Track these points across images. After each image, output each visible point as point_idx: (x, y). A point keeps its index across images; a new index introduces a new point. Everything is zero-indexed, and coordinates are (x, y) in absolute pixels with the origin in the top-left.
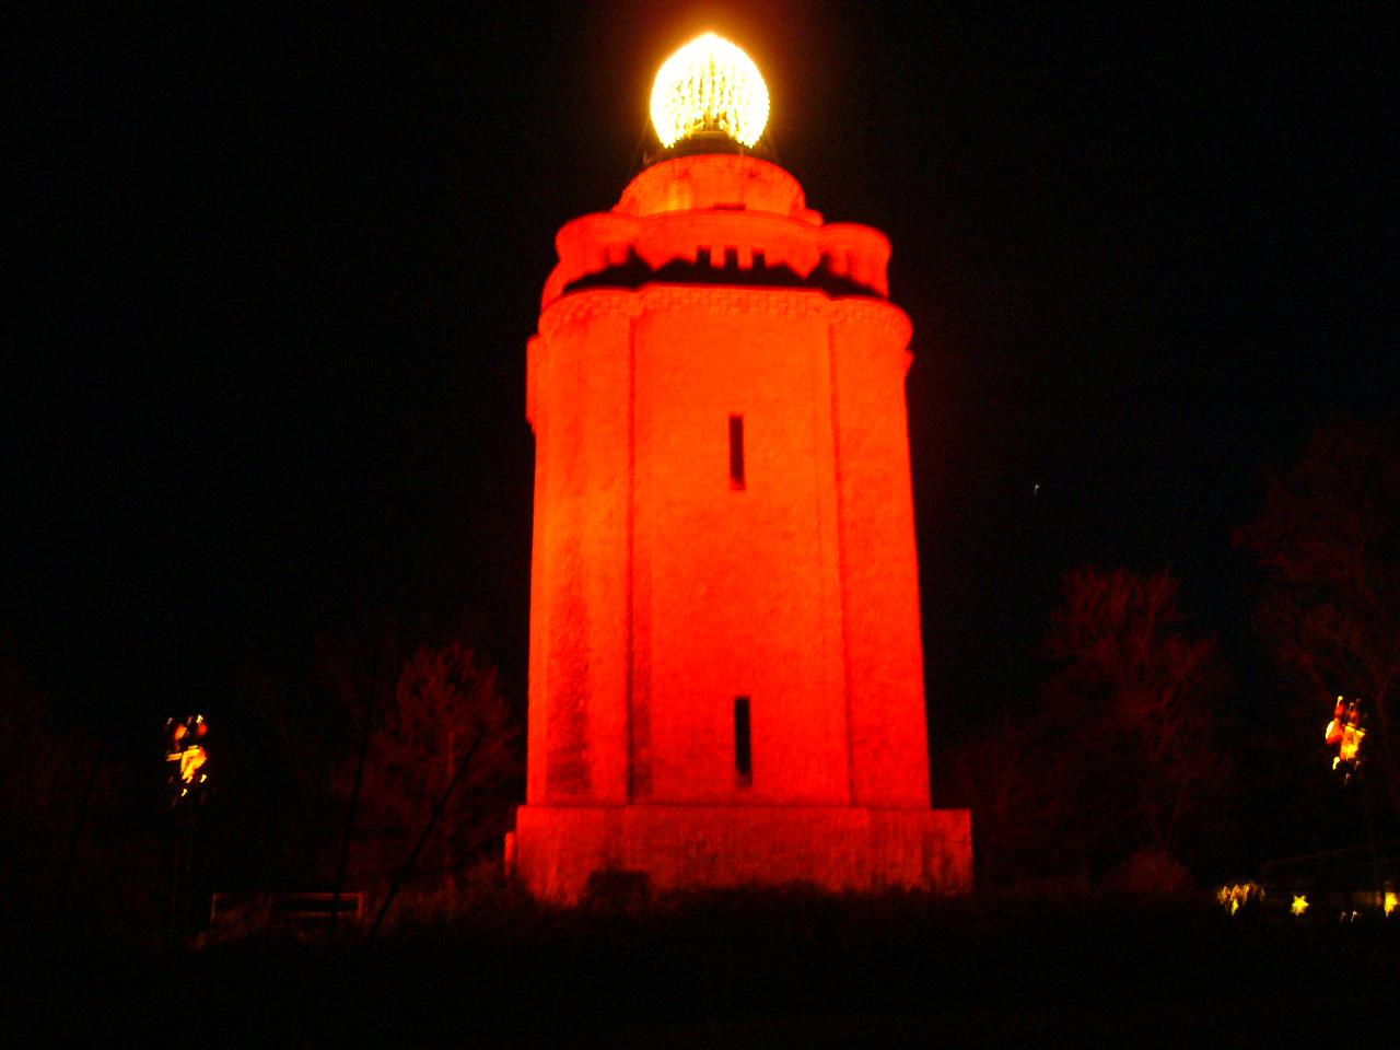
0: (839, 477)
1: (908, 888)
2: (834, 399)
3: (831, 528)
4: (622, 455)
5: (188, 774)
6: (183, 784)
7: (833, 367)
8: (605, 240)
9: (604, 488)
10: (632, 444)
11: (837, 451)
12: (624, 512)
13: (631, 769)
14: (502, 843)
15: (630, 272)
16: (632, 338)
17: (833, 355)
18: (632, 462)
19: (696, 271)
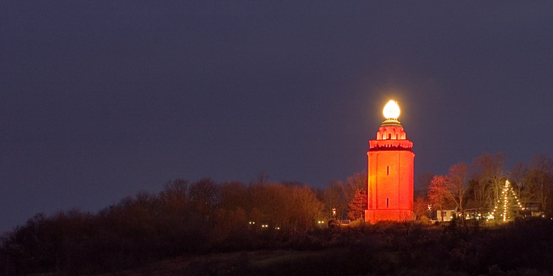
0: (399, 173)
1: (135, 198)
2: (399, 163)
3: (398, 179)
4: (376, 171)
5: (334, 213)
6: (526, 209)
7: (399, 159)
8: (374, 144)
9: (374, 175)
10: (377, 170)
11: (399, 169)
12: (376, 177)
13: (377, 206)
14: (467, 220)
15: (378, 148)
16: (377, 157)
17: (399, 158)
18: (377, 172)
19: (384, 149)
